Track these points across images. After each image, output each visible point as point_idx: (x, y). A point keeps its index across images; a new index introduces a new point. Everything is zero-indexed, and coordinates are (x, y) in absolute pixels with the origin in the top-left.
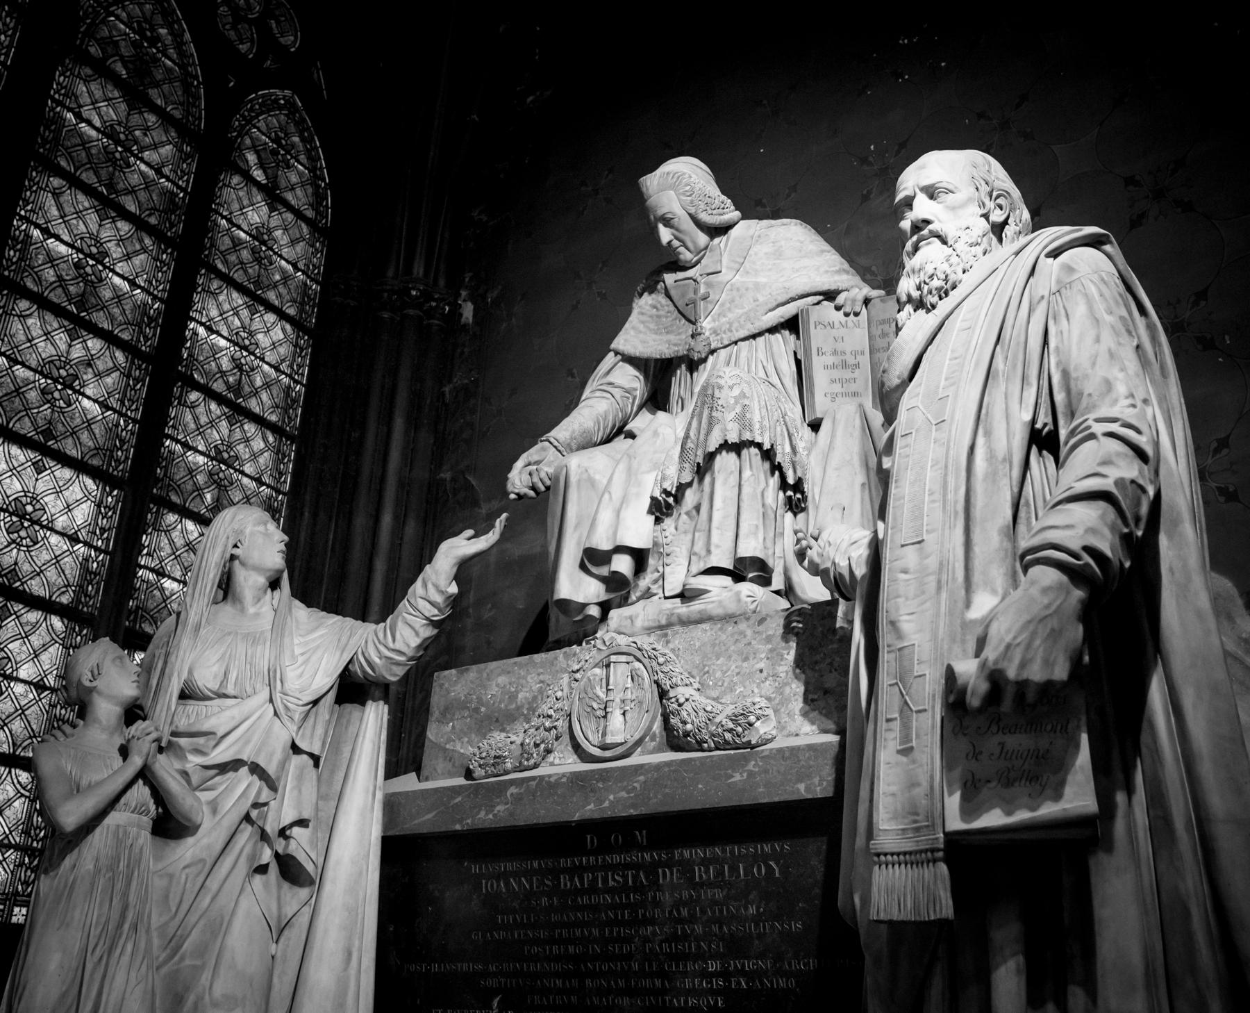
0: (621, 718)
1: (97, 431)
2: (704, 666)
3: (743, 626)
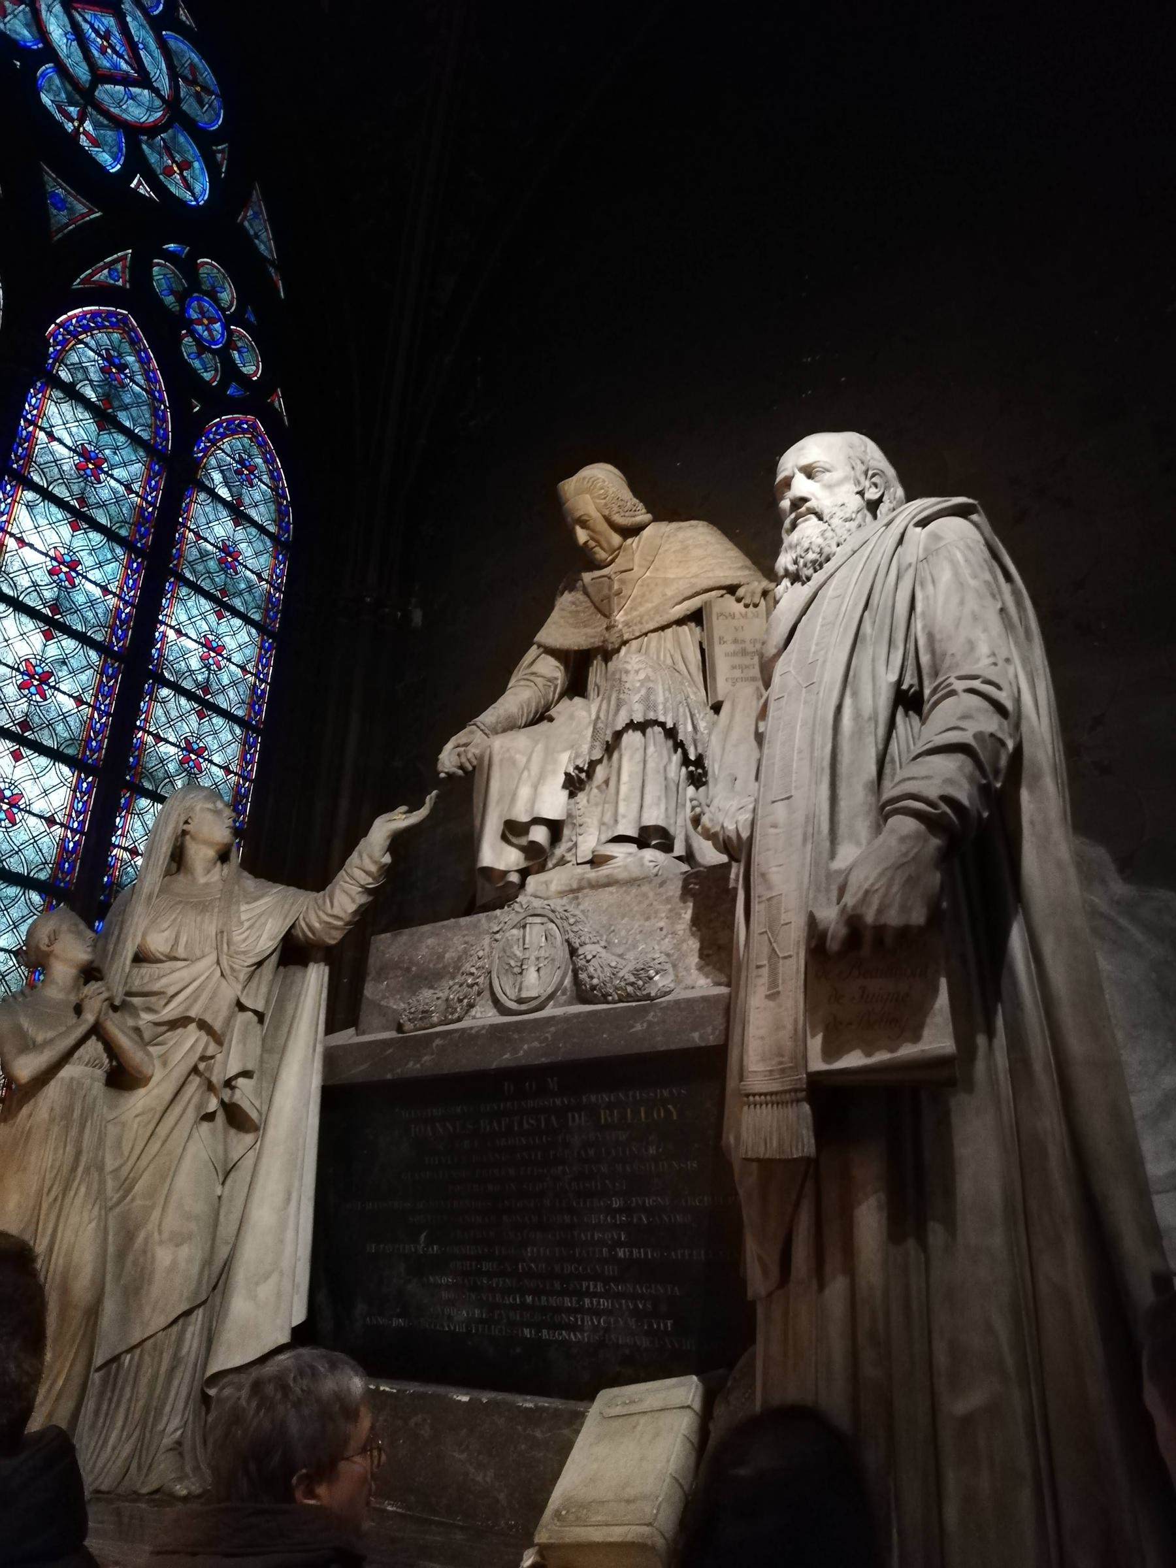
0: (535, 974)
1: (72, 723)
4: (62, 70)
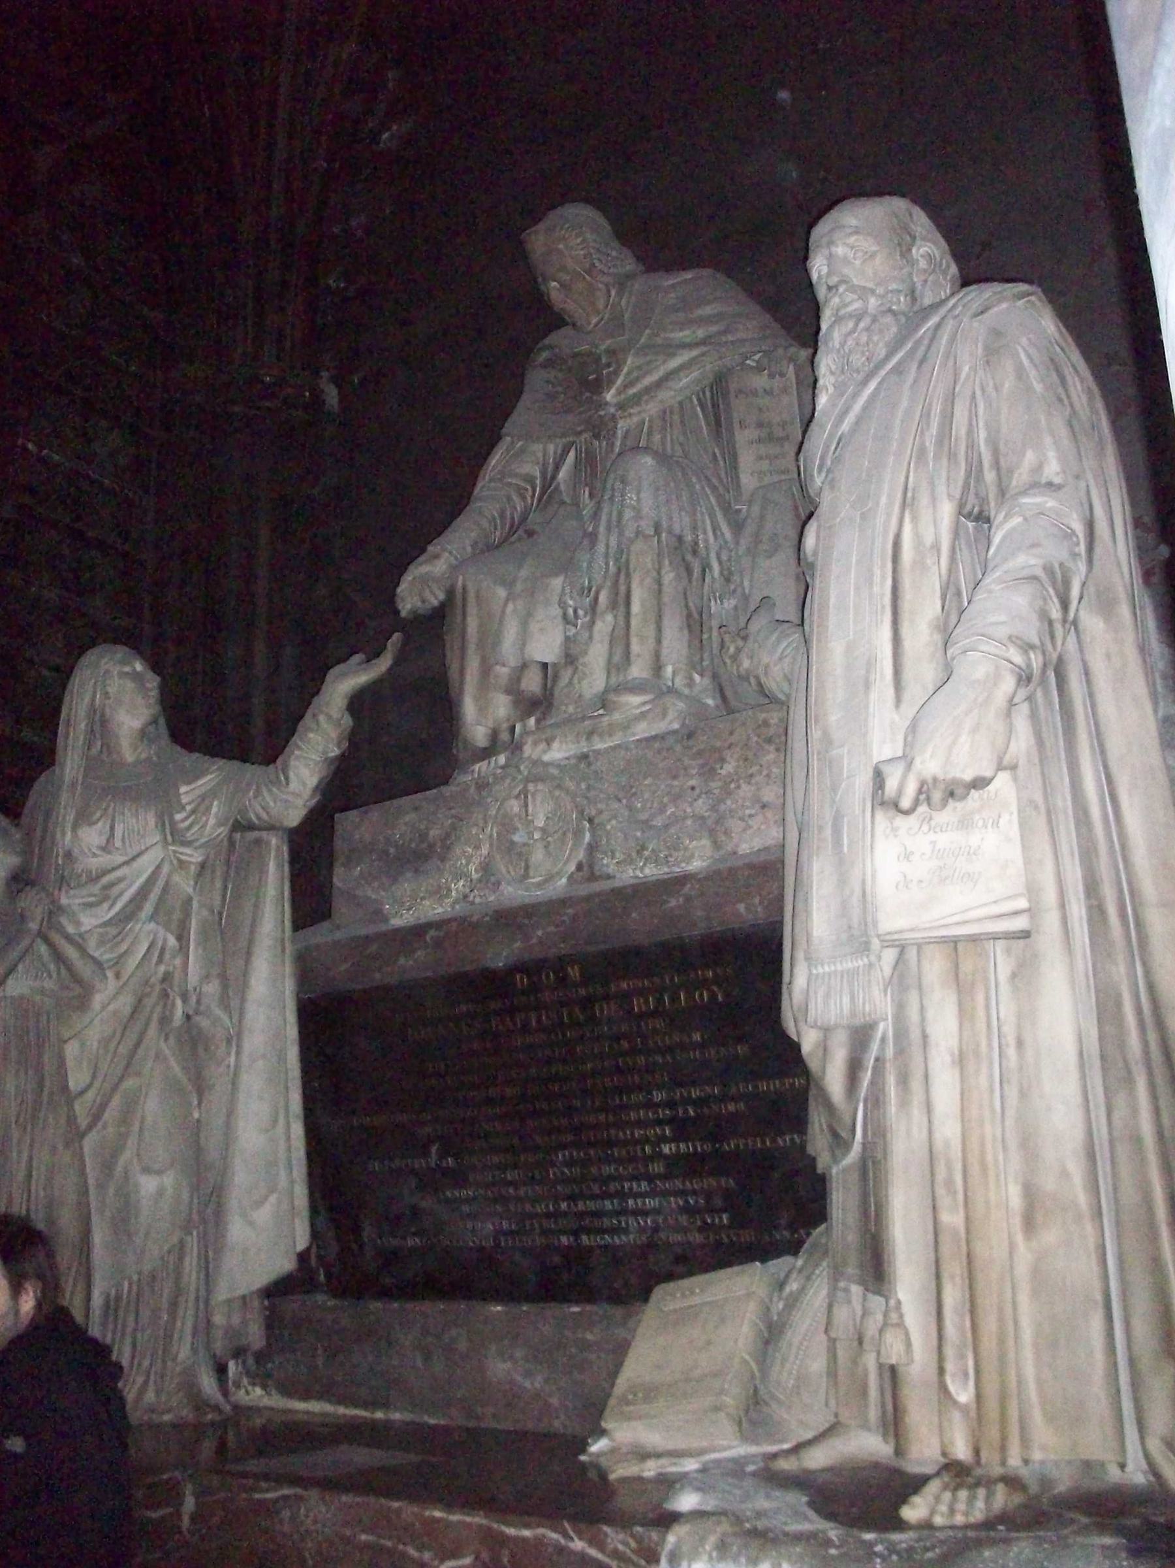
2: (632, 787)
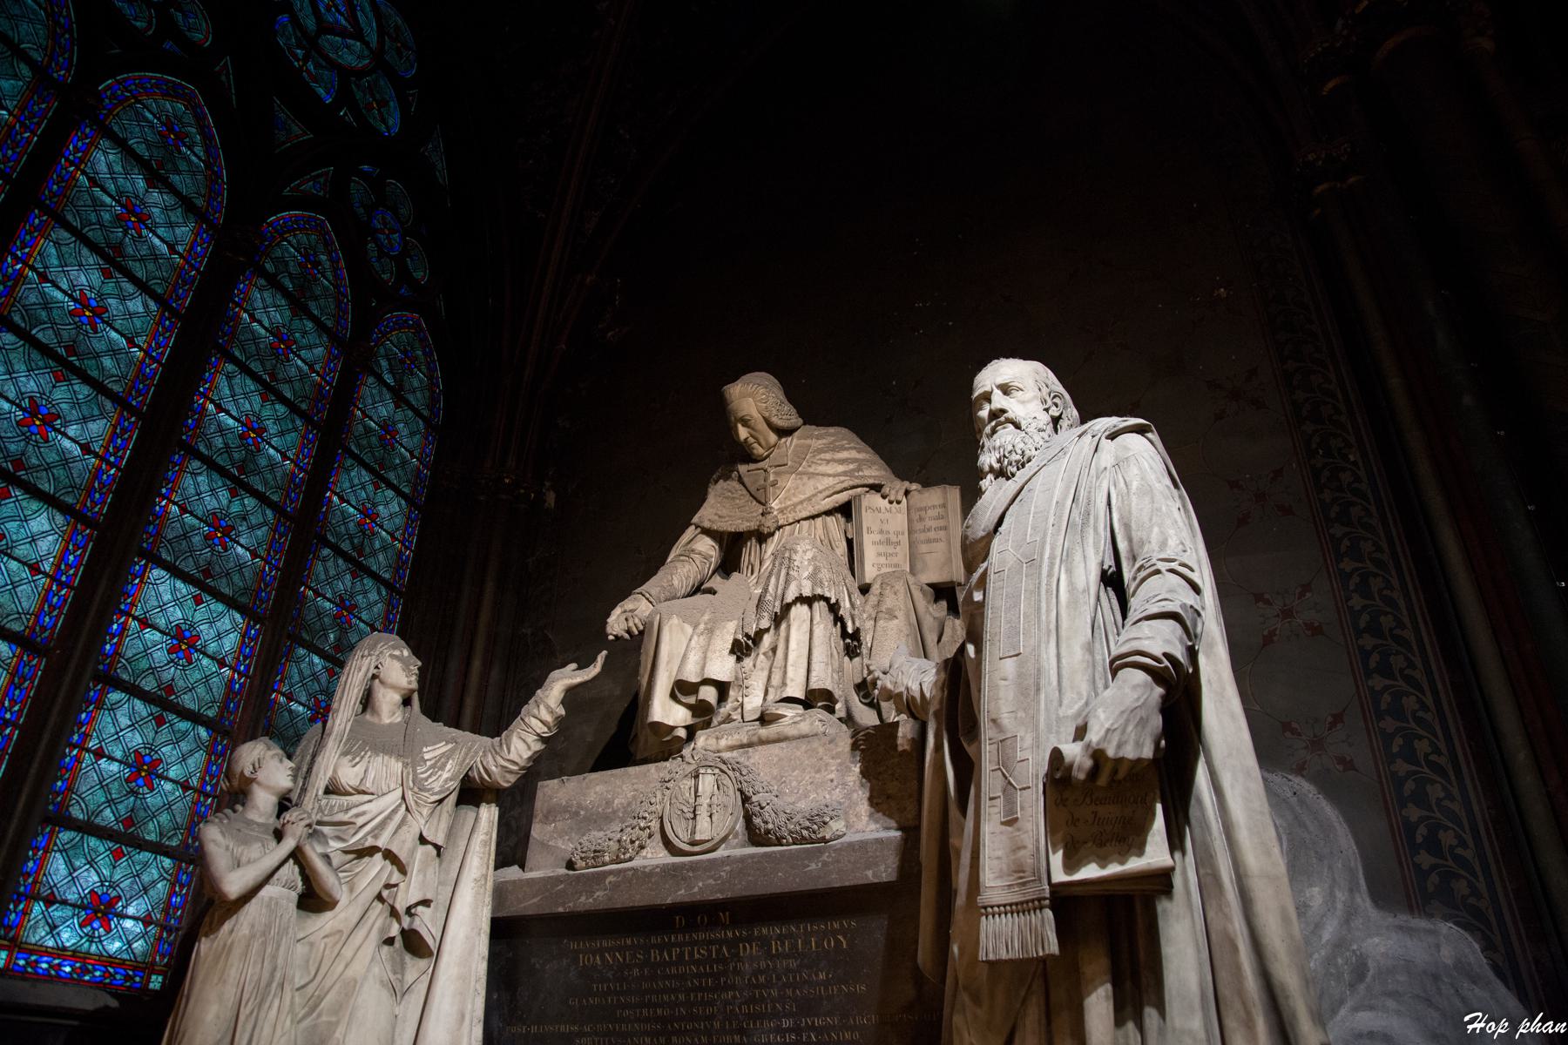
3: (816, 744)
4: (295, 21)
